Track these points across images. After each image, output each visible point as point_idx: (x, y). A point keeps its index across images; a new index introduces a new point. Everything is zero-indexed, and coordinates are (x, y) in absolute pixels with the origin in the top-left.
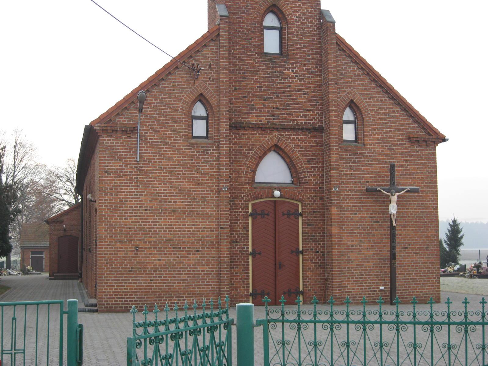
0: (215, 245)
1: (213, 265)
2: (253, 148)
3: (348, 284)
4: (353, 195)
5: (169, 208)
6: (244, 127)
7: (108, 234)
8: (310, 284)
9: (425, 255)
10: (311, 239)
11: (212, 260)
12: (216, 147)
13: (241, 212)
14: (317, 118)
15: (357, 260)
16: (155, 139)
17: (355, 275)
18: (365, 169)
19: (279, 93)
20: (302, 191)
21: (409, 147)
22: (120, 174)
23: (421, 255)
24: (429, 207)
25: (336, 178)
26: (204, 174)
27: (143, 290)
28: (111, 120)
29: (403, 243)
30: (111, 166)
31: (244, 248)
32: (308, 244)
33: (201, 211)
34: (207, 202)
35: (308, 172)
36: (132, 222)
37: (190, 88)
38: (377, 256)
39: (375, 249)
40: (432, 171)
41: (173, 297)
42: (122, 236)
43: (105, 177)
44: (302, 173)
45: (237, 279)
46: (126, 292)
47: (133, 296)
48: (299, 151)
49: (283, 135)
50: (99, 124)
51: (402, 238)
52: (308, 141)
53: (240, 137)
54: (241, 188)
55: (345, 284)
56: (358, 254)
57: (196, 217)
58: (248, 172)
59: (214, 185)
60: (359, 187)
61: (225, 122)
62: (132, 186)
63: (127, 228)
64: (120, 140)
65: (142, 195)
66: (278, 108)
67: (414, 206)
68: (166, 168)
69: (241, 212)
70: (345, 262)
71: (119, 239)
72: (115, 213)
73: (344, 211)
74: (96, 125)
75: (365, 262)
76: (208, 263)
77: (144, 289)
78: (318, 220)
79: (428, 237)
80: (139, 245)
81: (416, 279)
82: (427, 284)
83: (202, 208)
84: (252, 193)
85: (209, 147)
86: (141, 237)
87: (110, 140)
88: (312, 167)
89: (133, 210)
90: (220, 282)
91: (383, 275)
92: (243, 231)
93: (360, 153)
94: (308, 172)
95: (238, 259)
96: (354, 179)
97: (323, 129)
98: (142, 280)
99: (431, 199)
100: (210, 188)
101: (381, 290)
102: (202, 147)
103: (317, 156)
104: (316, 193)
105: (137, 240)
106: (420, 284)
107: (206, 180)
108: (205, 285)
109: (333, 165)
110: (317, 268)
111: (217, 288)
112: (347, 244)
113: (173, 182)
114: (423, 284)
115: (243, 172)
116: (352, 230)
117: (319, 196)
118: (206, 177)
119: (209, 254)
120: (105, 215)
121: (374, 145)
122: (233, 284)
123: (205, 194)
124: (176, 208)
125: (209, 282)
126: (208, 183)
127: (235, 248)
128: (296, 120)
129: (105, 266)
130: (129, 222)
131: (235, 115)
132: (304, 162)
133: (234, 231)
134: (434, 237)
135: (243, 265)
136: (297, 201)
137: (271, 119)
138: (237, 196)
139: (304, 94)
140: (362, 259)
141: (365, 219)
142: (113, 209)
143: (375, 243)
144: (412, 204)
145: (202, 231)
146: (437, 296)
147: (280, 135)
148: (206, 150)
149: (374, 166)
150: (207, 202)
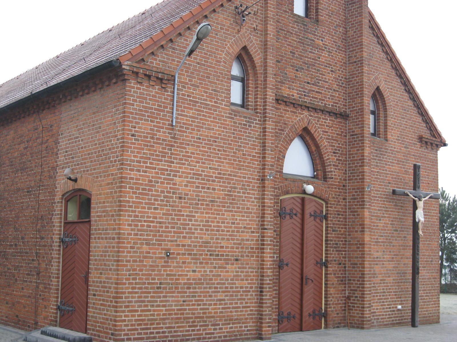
0: (255, 252)
2: (285, 128)
5: (208, 197)
7: (132, 230)
12: (259, 120)
16: (193, 97)
19: (310, 65)
22: (150, 142)
27: (174, 316)
28: (143, 60)
30: (139, 128)
35: (334, 165)
36: (164, 214)
37: (234, 36)
41: (208, 325)
42: (150, 235)
43: (132, 143)
46: (152, 320)
47: (162, 326)
48: (327, 139)
50: (129, 63)
57: (236, 212)
59: (256, 170)
62: (165, 161)
63: (157, 222)
64: (152, 92)
65: (175, 176)
66: (308, 83)
68: (205, 140)
71: (146, 240)
72: (143, 199)
74: (126, 63)
77: (176, 314)
80: (170, 249)
86: (174, 236)
87: (140, 89)
88: (337, 160)
89: (165, 197)
90: (261, 303)
97: (348, 116)
98: (173, 301)
101: (399, 310)
105: (169, 241)
111: (256, 311)
113: (213, 161)
120: (129, 202)
124: (214, 198)
129: (127, 279)
130: (159, 213)
136: (323, 200)
139: (332, 71)
142: (140, 193)
147: (311, 116)
148: (248, 122)
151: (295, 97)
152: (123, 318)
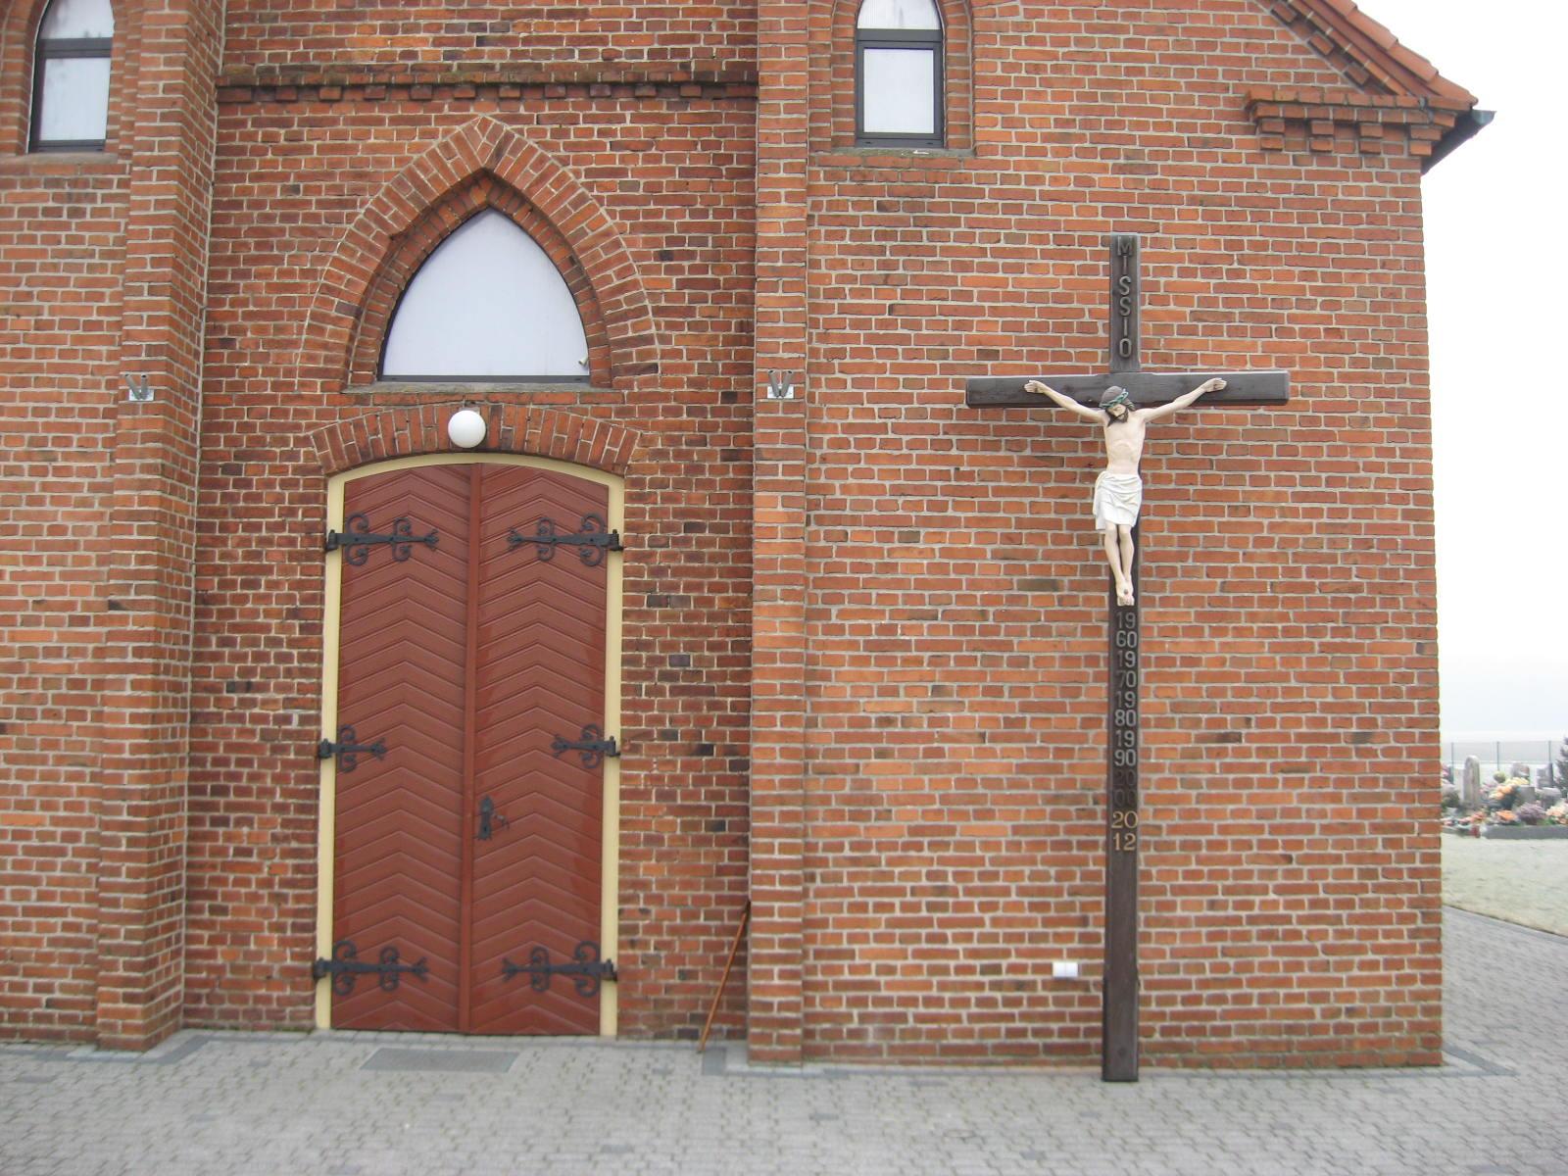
1: (79, 807)
3: (852, 938)
4: (896, 429)
6: (316, 88)
8: (654, 929)
9: (1347, 783)
10: (665, 676)
11: (71, 777)
13: (280, 527)
14: (722, 26)
15: (914, 800)
17: (900, 892)
18: (976, 282)
20: (620, 413)
21: (1250, 159)
23: (1322, 782)
24: (1377, 498)
25: (787, 332)
26: (50, 325)
29: (1207, 708)
31: (287, 719)
32: (648, 706)
33: (27, 516)
34: (58, 471)
35: (658, 311)
38: (1041, 784)
39: (1030, 738)
40: (1394, 294)
44: (625, 316)
45: (246, 883)
48: (613, 201)
49: (527, 120)
51: (1201, 677)
52: (662, 146)
53: (293, 138)
54: (288, 399)
55: (838, 938)
56: (923, 769)
58: (325, 318)
59: (103, 380)
60: (933, 384)
61: (164, 48)
67: (1279, 497)
69: (280, 527)
70: (838, 815)
73: (838, 520)
75: (963, 815)
76: (48, 795)
78: (710, 572)
79: (1365, 678)
81: (1287, 920)
82: (1358, 950)
83: (32, 501)
84: (345, 427)
85: (86, 184)
88: (682, 284)
91: (1074, 892)
92: (282, 628)
93: (945, 193)
94: (658, 311)
95: (253, 777)
96: (904, 340)
99: (1391, 452)
100: (79, 398)
101: (1064, 983)
102: (49, 183)
103: (713, 228)
104: (703, 427)
106: (1310, 951)
107: (63, 354)
108: (27, 911)
109: (774, 257)
110: (701, 841)
112: (850, 706)
114: (1329, 950)
115: (301, 317)
116: (890, 629)
117: (725, 441)
118: (61, 340)
119: (54, 745)
121: (1030, 151)
122: (224, 911)
123: (48, 427)
125: (50, 896)
126: (73, 369)
127: (241, 718)
128: (603, 41)
131: (274, 31)
132: (639, 256)
133: (235, 628)
134: (1405, 678)
135: (281, 808)
136: (594, 465)
137: (468, 42)
138: (260, 441)
140: (945, 799)
141: (970, 569)
143: (1026, 707)
144: (1266, 481)
145: (26, 621)
146: (1416, 1027)
147: (513, 119)
148: (69, 198)
149: (1033, 268)
150: (58, 471)
151: (420, 60)
152: (924, 913)
